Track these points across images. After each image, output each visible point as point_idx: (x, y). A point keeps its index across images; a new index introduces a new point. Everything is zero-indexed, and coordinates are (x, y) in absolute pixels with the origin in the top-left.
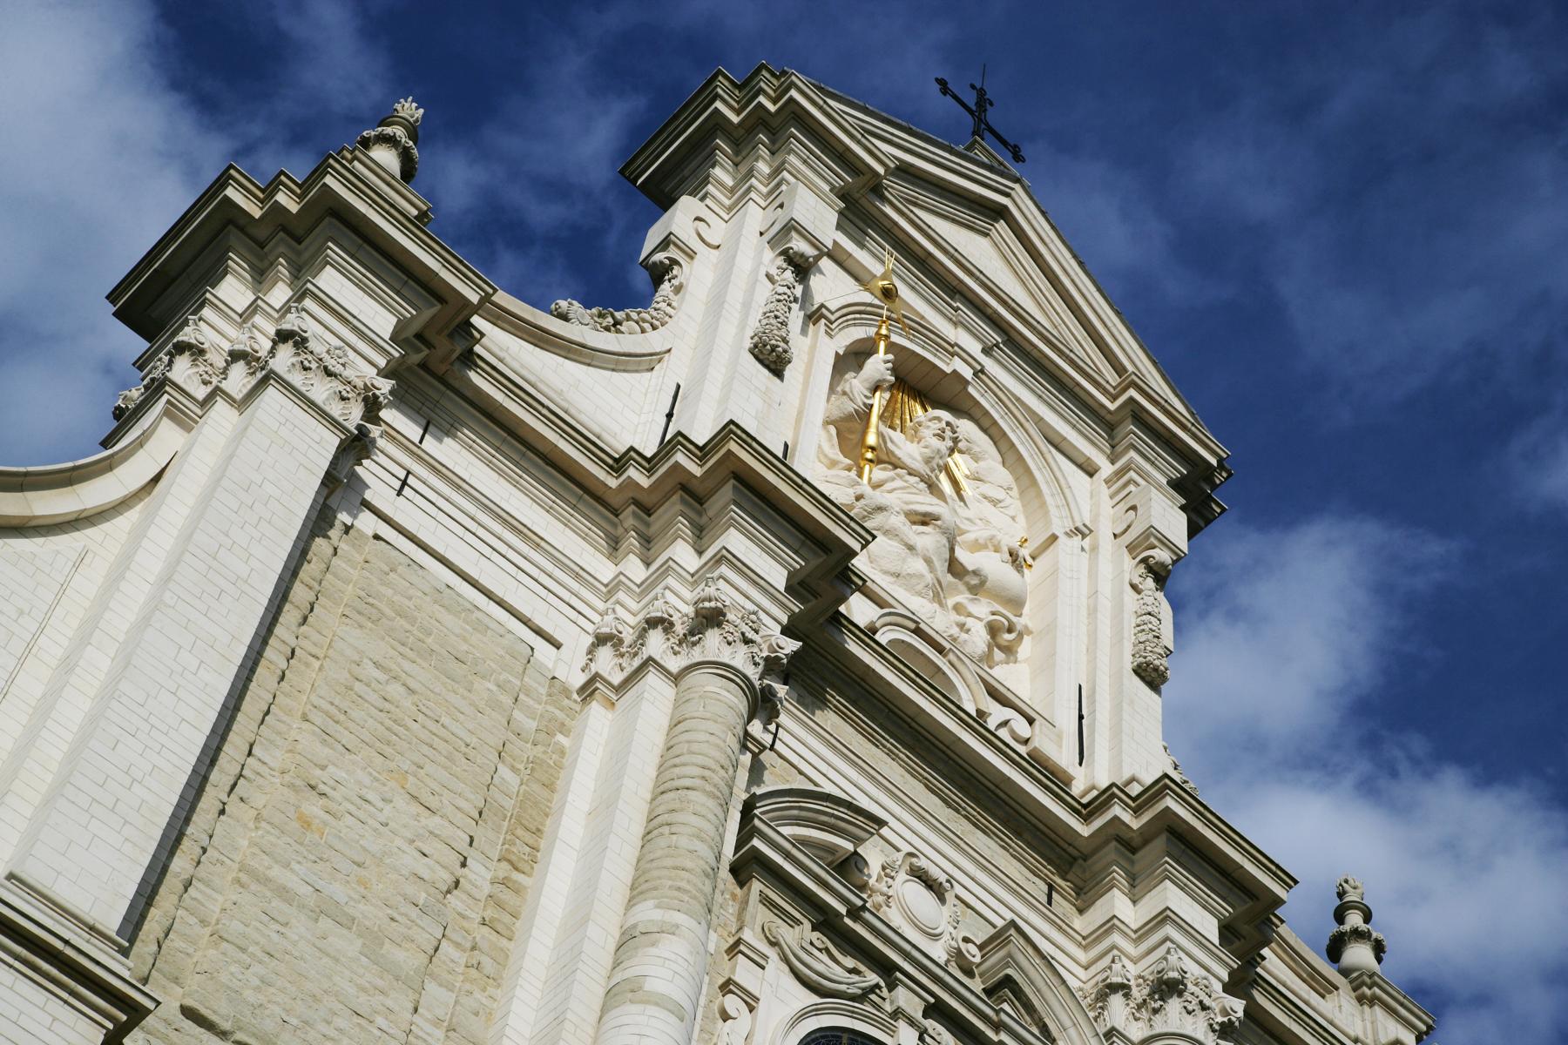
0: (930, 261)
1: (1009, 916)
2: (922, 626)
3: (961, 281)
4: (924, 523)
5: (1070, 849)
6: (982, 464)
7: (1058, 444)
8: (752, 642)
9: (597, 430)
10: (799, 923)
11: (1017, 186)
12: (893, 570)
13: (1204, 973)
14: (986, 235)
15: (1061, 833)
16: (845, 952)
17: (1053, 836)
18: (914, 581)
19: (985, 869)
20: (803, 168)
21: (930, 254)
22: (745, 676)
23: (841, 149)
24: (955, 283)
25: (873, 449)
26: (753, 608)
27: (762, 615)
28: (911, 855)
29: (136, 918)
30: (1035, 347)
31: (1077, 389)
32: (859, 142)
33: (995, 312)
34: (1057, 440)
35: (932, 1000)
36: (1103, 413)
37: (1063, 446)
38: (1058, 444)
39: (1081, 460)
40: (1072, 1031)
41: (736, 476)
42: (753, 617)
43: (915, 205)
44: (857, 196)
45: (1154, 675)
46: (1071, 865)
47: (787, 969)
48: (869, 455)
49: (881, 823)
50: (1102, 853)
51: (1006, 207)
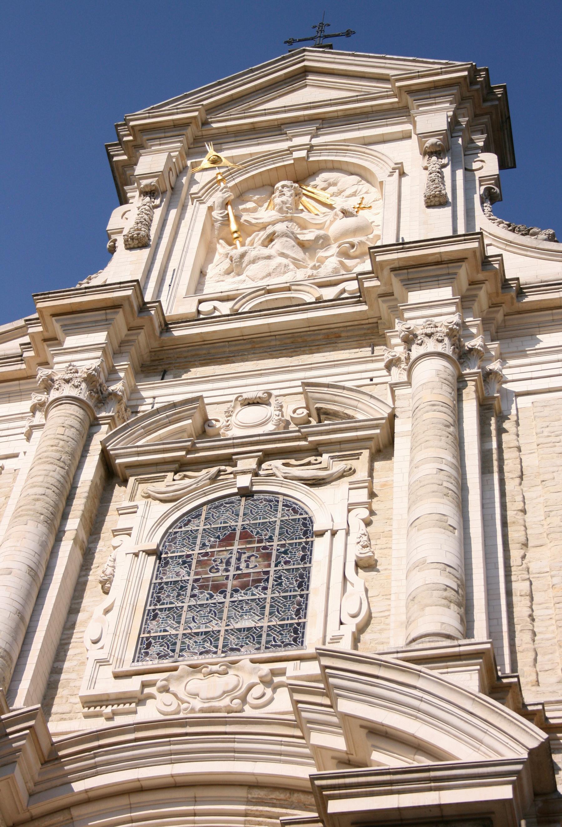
0: (256, 126)
1: (299, 383)
2: (268, 288)
3: (277, 120)
4: (272, 241)
5: (371, 321)
6: (339, 185)
7: (368, 142)
8: (432, 333)
9: (539, 280)
10: (165, 477)
11: (306, 53)
12: (265, 274)
13: (425, 320)
14: (306, 86)
15: (358, 318)
16: (199, 470)
17: (356, 323)
18: (278, 270)
19: (311, 369)
20: (162, 147)
21: (252, 123)
22: (67, 397)
23: (432, 85)
24: (276, 123)
25: (236, 232)
26: (67, 364)
27: (75, 363)
28: (237, 399)
29: (458, 657)
30: (337, 111)
31: (374, 109)
32: (177, 113)
33: (304, 116)
34: (381, 139)
35: (260, 453)
36: (396, 106)
37: (386, 138)
38: (368, 142)
39: (401, 136)
40: (360, 405)
41: (53, 315)
42: (71, 367)
43: (251, 108)
44: (200, 133)
45: (437, 199)
46: (377, 327)
47: (158, 502)
48: (235, 235)
49: (200, 398)
50: (381, 309)
51: (305, 66)
